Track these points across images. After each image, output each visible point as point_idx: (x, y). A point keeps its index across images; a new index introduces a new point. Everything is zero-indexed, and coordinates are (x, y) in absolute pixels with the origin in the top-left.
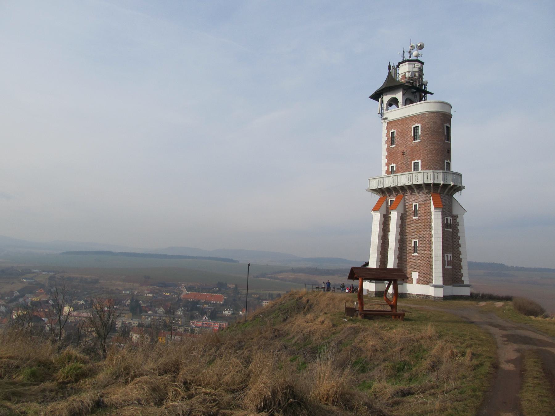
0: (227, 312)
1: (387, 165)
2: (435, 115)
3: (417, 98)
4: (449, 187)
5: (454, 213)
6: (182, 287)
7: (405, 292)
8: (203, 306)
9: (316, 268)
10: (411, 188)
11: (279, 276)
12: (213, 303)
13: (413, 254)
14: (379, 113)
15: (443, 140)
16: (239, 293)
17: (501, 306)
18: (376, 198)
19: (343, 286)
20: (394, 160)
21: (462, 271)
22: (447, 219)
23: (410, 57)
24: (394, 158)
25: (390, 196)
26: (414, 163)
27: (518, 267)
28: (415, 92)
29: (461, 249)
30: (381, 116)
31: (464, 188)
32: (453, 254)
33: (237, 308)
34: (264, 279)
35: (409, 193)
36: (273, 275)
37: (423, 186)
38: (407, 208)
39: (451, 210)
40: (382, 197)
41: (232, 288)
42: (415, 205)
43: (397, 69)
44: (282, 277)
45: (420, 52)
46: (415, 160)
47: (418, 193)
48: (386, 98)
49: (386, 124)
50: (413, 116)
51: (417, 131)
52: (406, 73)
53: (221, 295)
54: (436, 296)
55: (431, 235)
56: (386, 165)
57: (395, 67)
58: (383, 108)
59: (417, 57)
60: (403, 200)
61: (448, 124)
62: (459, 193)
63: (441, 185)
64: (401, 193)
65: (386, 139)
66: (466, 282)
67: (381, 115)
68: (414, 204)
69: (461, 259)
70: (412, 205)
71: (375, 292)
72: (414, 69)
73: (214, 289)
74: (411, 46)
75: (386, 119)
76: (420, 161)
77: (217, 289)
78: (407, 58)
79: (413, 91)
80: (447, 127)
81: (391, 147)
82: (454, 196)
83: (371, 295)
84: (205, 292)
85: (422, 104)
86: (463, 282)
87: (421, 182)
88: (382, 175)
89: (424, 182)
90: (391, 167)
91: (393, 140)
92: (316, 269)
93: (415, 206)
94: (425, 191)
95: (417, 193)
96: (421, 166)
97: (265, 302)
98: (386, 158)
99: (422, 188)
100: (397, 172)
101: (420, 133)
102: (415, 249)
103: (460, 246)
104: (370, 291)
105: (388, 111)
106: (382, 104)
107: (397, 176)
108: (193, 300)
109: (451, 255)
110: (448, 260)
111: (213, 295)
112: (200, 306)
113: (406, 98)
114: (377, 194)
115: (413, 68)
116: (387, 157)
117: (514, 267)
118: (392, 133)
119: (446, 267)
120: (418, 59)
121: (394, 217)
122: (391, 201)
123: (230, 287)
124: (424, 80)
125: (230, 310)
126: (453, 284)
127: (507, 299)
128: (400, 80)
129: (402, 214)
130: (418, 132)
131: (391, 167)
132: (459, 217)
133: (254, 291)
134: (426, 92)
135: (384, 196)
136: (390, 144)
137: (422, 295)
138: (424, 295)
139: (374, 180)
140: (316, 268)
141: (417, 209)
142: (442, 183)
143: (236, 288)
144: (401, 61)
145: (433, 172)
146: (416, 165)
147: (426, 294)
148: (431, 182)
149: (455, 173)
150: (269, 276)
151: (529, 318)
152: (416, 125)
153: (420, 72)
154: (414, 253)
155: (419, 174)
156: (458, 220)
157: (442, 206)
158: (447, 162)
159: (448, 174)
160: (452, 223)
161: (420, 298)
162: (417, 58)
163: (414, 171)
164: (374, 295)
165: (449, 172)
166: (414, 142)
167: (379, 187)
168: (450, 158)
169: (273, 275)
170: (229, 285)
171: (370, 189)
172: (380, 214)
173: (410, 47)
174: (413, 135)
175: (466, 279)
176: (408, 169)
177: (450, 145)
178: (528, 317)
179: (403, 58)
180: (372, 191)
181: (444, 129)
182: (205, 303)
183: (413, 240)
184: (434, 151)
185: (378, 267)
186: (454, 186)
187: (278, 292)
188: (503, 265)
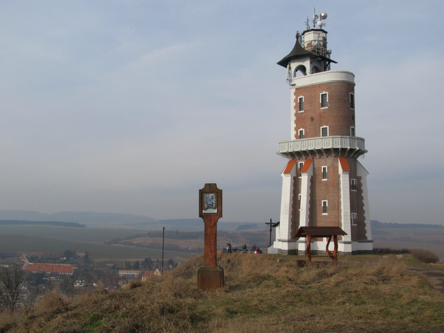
0: (78, 284)
1: (296, 129)
2: (341, 84)
3: (322, 66)
4: (355, 151)
5: (358, 175)
6: (23, 257)
7: (317, 250)
8: (50, 278)
9: (177, 231)
10: (320, 152)
11: (135, 242)
12: (62, 275)
13: (323, 214)
14: (287, 80)
15: (349, 107)
16: (90, 262)
17: (402, 257)
18: (286, 160)
19: (245, 247)
20: (302, 125)
21: (366, 228)
22: (353, 181)
23: (314, 26)
25: (299, 159)
27: (392, 223)
28: (321, 61)
29: (364, 208)
30: (289, 82)
31: (367, 152)
33: (90, 280)
34: (118, 245)
35: (317, 156)
36: (128, 241)
37: (332, 150)
38: (316, 170)
39: (355, 172)
40: (292, 160)
41: (81, 256)
42: (324, 168)
43: (302, 36)
44: (138, 242)
45: (323, 21)
46: (323, 126)
47: (327, 157)
48: (294, 65)
49: (294, 90)
50: (321, 84)
51: (325, 99)
52: (312, 42)
53: (70, 265)
54: (346, 251)
55: (339, 196)
56: (295, 130)
57: (301, 34)
58: (291, 74)
59: (321, 26)
60: (312, 163)
61: (352, 92)
62: (362, 156)
63: (348, 150)
64: (310, 157)
65: (294, 104)
66: (369, 238)
67: (289, 81)
68: (323, 167)
69: (365, 217)
70: (321, 168)
71: (288, 250)
72: (319, 38)
73: (61, 258)
74: (315, 16)
75: (294, 85)
76: (328, 127)
77: (65, 258)
78: (312, 27)
79: (319, 59)
81: (299, 112)
82: (357, 159)
83: (284, 253)
84: (50, 263)
85: (329, 73)
86: (366, 238)
87: (330, 147)
88: (291, 140)
89: (333, 147)
90: (300, 131)
91: (301, 105)
92: (177, 232)
93: (324, 169)
94: (333, 155)
95: (325, 156)
96: (329, 131)
97: (122, 271)
98: (295, 123)
99: (331, 152)
100: (306, 136)
101: (327, 101)
102: (325, 209)
103: (364, 206)
104: (283, 250)
105: (296, 78)
106: (290, 70)
107: (307, 141)
108: (38, 272)
109: (356, 214)
110: (356, 218)
111: (61, 266)
112: (46, 278)
113: (314, 65)
114: (286, 157)
115: (318, 37)
116: (296, 122)
117: (388, 223)
118: (300, 99)
120: (322, 29)
121: (305, 179)
122: (300, 164)
123: (79, 255)
124: (328, 49)
125: (82, 282)
127: (404, 252)
128: (306, 48)
129: (312, 177)
130: (326, 99)
131: (300, 131)
132: (362, 178)
133: (108, 260)
134: (330, 61)
135: (293, 159)
136: (299, 109)
139: (284, 144)
140: (177, 231)
141: (326, 171)
142: (349, 148)
143: (87, 256)
144: (306, 30)
145: (341, 138)
146: (324, 130)
148: (339, 147)
149: (360, 138)
150: (123, 241)
151: (430, 264)
152: (324, 93)
153: (324, 41)
154: (324, 212)
155: (328, 139)
156: (362, 181)
157: (349, 169)
158: (352, 128)
159: (354, 140)
162: (321, 28)
163: (322, 136)
164: (287, 254)
165: (354, 137)
166: (322, 108)
167: (290, 151)
168: (353, 123)
169: (128, 241)
170: (78, 254)
171: (280, 152)
172: (291, 176)
173: (314, 16)
174: (321, 102)
175: (369, 235)
176: (316, 134)
177: (353, 112)
178: (429, 264)
179: (307, 27)
180: (282, 154)
181: (349, 97)
182: (52, 275)
183: (323, 201)
184: (341, 118)
185: (307, 226)
186: (359, 150)
187: (136, 260)
188: (377, 221)
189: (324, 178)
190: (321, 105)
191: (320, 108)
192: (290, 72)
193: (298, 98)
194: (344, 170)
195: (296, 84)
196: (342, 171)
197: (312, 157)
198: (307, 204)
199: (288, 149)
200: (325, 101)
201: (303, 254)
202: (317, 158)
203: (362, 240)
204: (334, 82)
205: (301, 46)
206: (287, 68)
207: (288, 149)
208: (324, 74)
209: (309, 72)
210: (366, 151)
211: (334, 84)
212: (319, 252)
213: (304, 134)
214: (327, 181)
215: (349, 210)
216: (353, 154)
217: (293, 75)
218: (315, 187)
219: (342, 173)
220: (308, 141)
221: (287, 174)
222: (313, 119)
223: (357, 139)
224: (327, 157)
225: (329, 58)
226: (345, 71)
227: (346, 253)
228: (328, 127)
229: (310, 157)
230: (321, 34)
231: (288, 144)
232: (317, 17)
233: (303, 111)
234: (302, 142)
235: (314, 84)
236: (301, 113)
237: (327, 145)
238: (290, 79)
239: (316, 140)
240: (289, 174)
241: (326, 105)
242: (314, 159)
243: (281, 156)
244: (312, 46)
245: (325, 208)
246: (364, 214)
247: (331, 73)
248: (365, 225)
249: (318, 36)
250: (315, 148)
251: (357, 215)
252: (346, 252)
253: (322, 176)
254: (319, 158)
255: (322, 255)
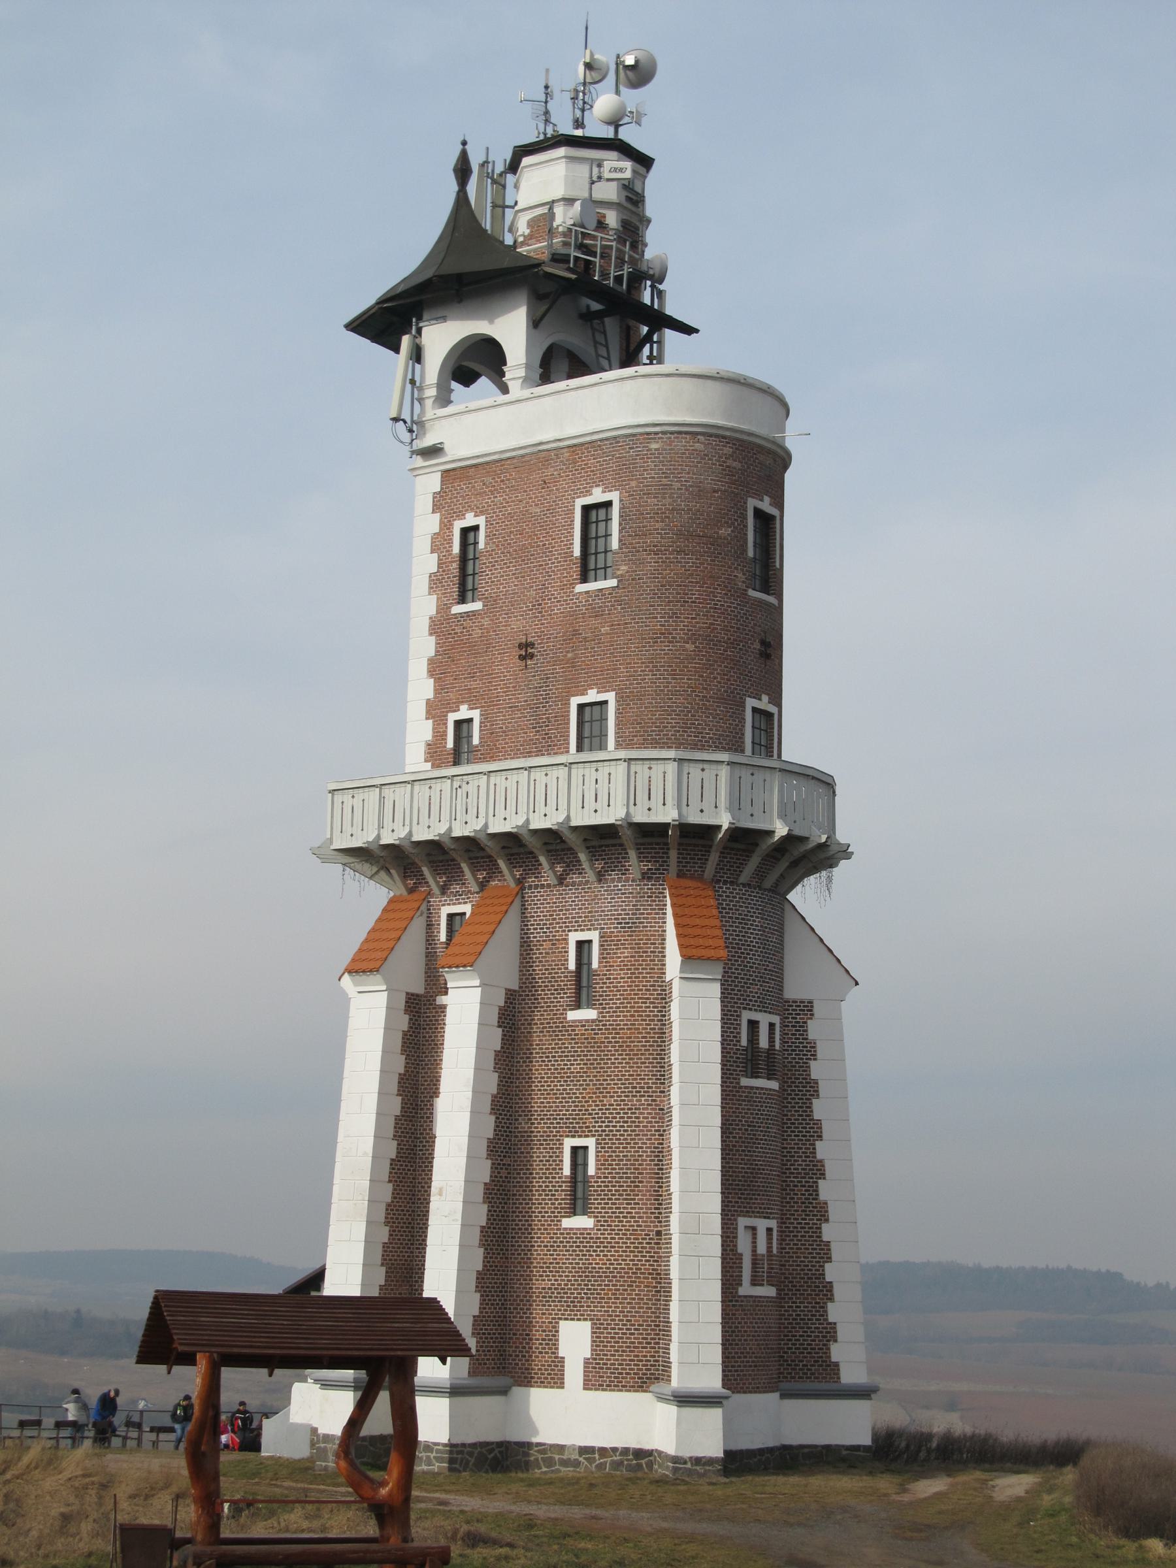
1: (436, 710)
4: (765, 845)
5: (793, 990)
9: (78, 1311)
14: (396, 420)
21: (834, 1312)
22: (753, 1025)
24: (472, 676)
25: (444, 890)
26: (581, 707)
28: (599, 315)
29: (826, 1190)
30: (406, 437)
32: (782, 1223)
37: (627, 835)
39: (776, 975)
40: (405, 893)
43: (510, 179)
45: (632, 98)
46: (583, 693)
47: (600, 876)
49: (431, 483)
50: (582, 444)
51: (601, 532)
54: (686, 1453)
57: (499, 168)
58: (421, 389)
59: (615, 123)
64: (507, 876)
66: (851, 1375)
67: (411, 431)
68: (574, 937)
74: (589, 66)
75: (433, 451)
76: (610, 697)
78: (567, 129)
79: (588, 307)
80: (758, 513)
81: (458, 609)
87: (611, 815)
89: (628, 814)
90: (458, 723)
91: (470, 571)
92: (78, 1320)
93: (583, 946)
94: (634, 864)
95: (591, 875)
98: (431, 673)
100: (489, 753)
101: (615, 544)
102: (580, 1194)
103: (823, 1176)
106: (417, 366)
109: (773, 1224)
110: (769, 1248)
115: (593, 183)
116: (436, 668)
118: (465, 531)
119: (746, 1289)
122: (451, 917)
126: (784, 1385)
128: (523, 244)
129: (511, 995)
130: (607, 535)
131: (458, 723)
134: (661, 321)
135: (411, 891)
137: (614, 1450)
138: (626, 1451)
139: (360, 795)
140: (78, 1311)
145: (681, 761)
146: (591, 714)
147: (634, 1444)
148: (667, 815)
153: (629, 206)
156: (814, 1030)
157: (723, 953)
158: (755, 710)
160: (777, 1047)
161: (601, 1467)
162: (616, 132)
163: (580, 749)
166: (581, 588)
167: (387, 839)
173: (581, 68)
174: (577, 551)
177: (776, 613)
183: (569, 1143)
185: (375, 1293)
186: (790, 839)
188: (1117, 1276)
189: (578, 1006)
190: (575, 571)
191: (573, 585)
192: (417, 378)
193: (452, 525)
194: (690, 958)
195: (447, 447)
196: (679, 959)
197: (514, 876)
198: (470, 1157)
199: (381, 826)
200: (601, 548)
201: (436, 1467)
202: (543, 886)
203: (817, 1386)
204: (656, 433)
205: (480, 226)
206: (396, 349)
207: (381, 826)
208: (603, 387)
209: (522, 373)
210: (845, 853)
211: (654, 446)
212: (540, 1456)
213: (476, 740)
214: (593, 1021)
215: (714, 1203)
216: (754, 862)
217: (431, 392)
218: (529, 1059)
219: (681, 972)
220: (493, 779)
221: (364, 977)
222: (530, 650)
223: (777, 774)
224: (600, 881)
225: (656, 307)
226: (723, 374)
227: (689, 1466)
228: (610, 697)
229: (507, 876)
230: (607, 165)
231: (382, 799)
232: (596, 76)
233: (477, 606)
234: (456, 785)
235: (541, 444)
236: (467, 614)
237: (598, 806)
238: (415, 418)
239: (538, 775)
240: (378, 977)
241: (605, 568)
242: (530, 887)
243: (340, 867)
244: (551, 232)
245: (580, 1186)
246: (824, 1226)
247: (641, 380)
248: (831, 1291)
249: (591, 177)
250: (528, 821)
251: (775, 1233)
252: (691, 1458)
253: (571, 991)
254: (555, 886)
255: (558, 1471)
